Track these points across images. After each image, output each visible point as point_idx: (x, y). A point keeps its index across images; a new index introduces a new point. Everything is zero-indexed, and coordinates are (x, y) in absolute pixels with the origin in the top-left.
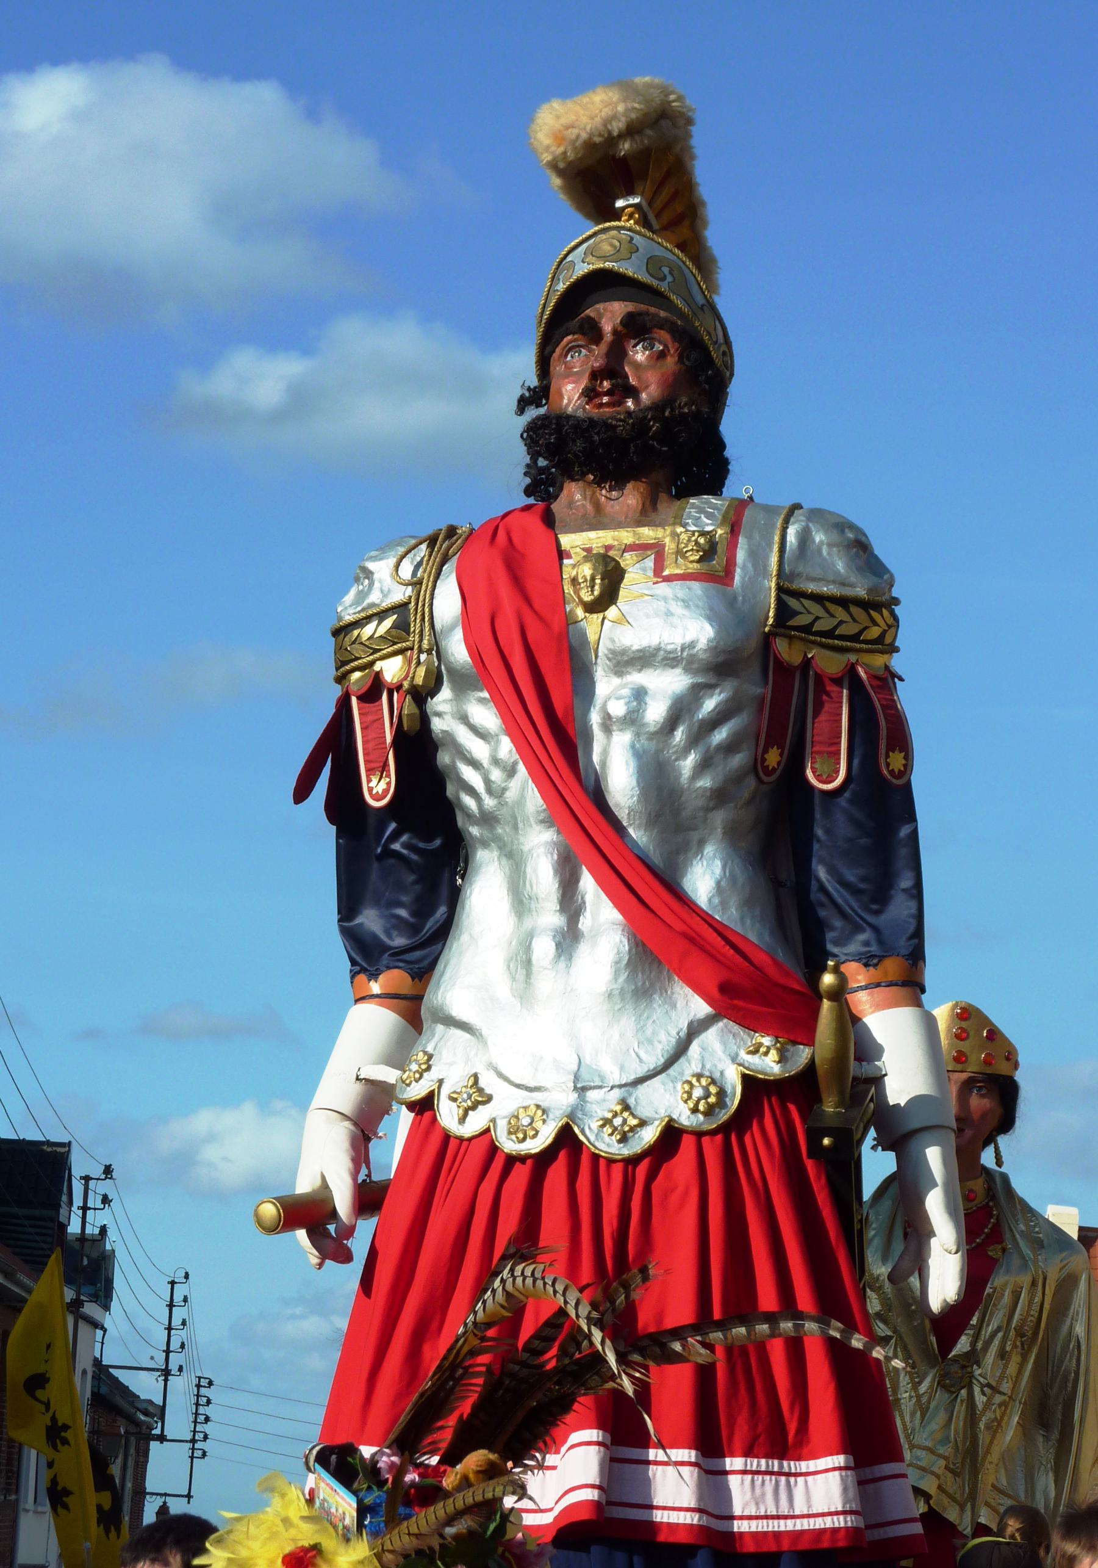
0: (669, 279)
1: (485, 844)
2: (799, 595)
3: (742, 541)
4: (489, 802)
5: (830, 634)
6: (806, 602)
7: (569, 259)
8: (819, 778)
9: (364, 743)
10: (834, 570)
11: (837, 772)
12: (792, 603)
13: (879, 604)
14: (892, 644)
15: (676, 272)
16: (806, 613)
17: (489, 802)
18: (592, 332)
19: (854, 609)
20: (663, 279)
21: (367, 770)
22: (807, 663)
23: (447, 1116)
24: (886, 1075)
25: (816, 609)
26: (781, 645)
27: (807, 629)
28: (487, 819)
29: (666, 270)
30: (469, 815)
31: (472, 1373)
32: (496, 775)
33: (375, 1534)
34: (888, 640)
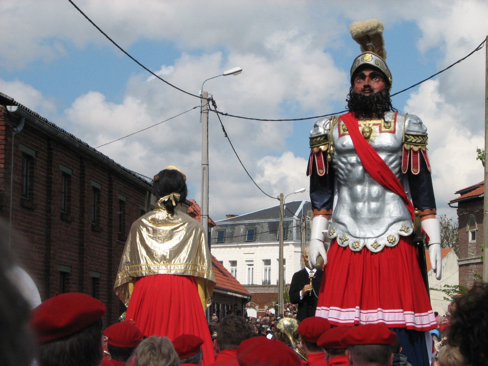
1: (344, 185)
18: (363, 77)
28: (345, 180)
32: (347, 172)
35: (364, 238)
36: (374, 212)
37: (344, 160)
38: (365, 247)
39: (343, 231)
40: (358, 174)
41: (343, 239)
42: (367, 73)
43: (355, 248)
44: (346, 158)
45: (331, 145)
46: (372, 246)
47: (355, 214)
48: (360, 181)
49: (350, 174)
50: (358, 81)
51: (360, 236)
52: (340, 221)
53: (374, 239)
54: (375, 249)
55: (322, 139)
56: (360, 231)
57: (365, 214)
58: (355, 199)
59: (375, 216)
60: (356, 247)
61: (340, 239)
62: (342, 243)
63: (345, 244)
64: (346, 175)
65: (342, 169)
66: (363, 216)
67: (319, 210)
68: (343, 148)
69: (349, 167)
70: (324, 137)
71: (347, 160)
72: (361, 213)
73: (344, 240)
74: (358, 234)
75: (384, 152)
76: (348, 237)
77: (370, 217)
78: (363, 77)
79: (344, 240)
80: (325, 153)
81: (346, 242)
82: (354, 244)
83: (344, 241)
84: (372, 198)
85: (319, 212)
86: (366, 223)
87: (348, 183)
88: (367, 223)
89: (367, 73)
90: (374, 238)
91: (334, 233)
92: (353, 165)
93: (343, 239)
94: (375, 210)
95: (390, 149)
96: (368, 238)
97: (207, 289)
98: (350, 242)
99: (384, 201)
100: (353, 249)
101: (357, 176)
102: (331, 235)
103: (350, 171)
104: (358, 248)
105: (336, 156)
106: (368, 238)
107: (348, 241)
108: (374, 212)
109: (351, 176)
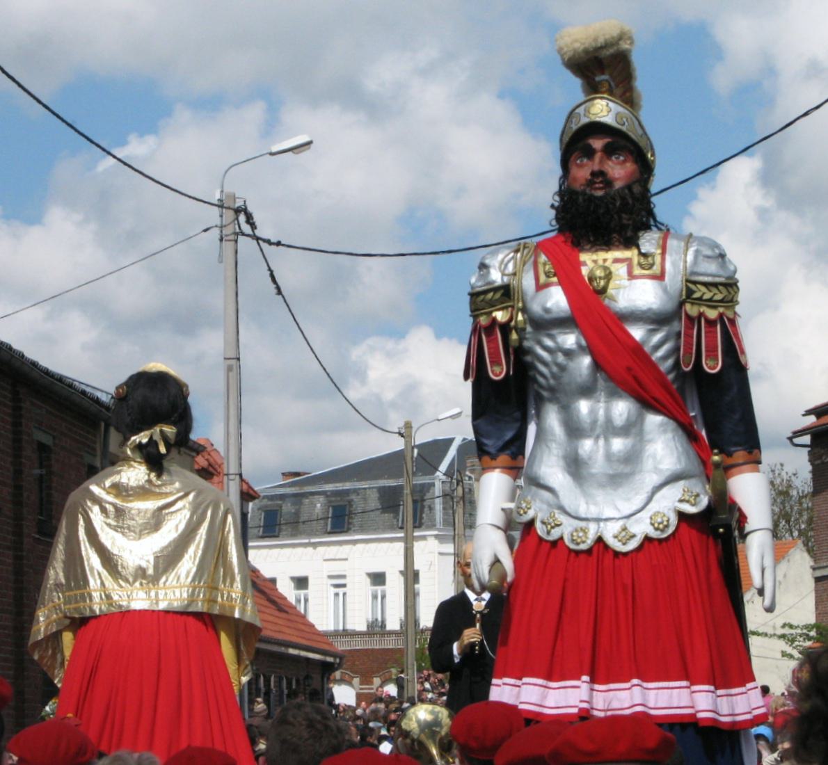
0: (626, 124)
1: (550, 400)
2: (695, 283)
3: (668, 257)
4: (552, 382)
5: (710, 300)
6: (699, 286)
7: (577, 111)
8: (710, 368)
9: (489, 349)
10: (710, 269)
11: (717, 364)
12: (691, 286)
13: (731, 285)
14: (737, 301)
15: (629, 120)
16: (700, 291)
17: (552, 382)
18: (590, 153)
19: (721, 288)
20: (624, 124)
21: (491, 362)
22: (701, 315)
23: (540, 529)
24: (735, 272)
25: (703, 289)
26: (688, 307)
27: (700, 299)
28: (552, 390)
29: (625, 120)
30: (541, 386)
31: (119, 582)
32: (555, 369)
33: (413, 740)
34: (735, 299)
37: (549, 342)
38: (600, 540)
40: (580, 375)
42: (598, 144)
43: (578, 544)
44: (552, 337)
45: (519, 310)
47: (575, 466)
48: (587, 391)
49: (564, 374)
50: (578, 162)
51: (589, 516)
52: (542, 482)
53: (621, 523)
54: (624, 544)
55: (498, 295)
56: (587, 503)
57: (599, 465)
58: (574, 430)
60: (579, 540)
61: (543, 523)
62: (548, 533)
63: (555, 534)
64: (554, 376)
65: (545, 364)
66: (594, 471)
67: (493, 457)
68: (547, 316)
69: (561, 358)
73: (553, 524)
75: (641, 323)
76: (561, 518)
77: (611, 472)
78: (590, 153)
79: (553, 524)
80: (506, 328)
81: (557, 529)
82: (575, 534)
83: (553, 528)
84: (614, 428)
85: (494, 463)
86: (602, 486)
87: (558, 395)
90: (620, 520)
92: (568, 353)
93: (549, 524)
95: (653, 317)
96: (607, 520)
98: (566, 530)
100: (572, 546)
101: (579, 380)
103: (562, 368)
104: (584, 542)
105: (529, 333)
107: (561, 527)
109: (566, 378)
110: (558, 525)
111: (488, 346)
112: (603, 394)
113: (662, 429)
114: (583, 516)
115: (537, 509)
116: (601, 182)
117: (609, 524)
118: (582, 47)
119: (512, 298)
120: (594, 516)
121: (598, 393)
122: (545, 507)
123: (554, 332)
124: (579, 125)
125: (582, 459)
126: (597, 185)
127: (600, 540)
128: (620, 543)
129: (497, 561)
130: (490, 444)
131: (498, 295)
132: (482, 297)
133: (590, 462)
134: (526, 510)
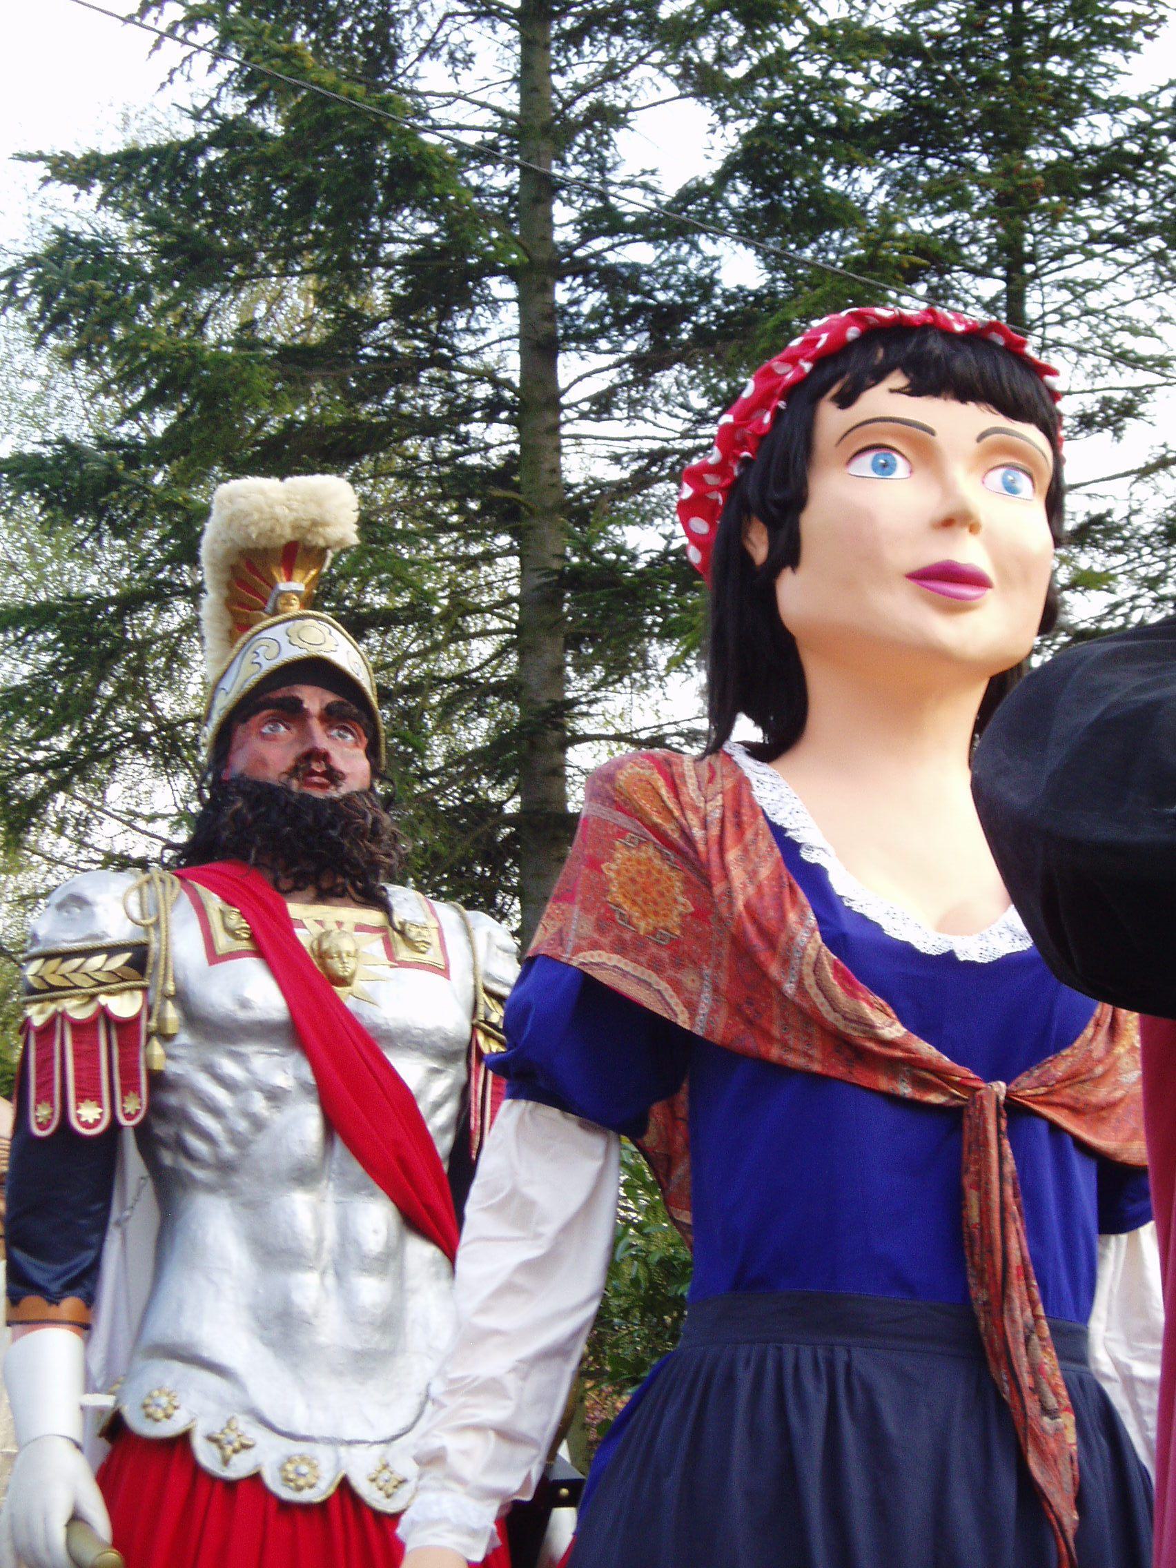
1: (211, 1189)
4: (228, 1150)
18: (293, 712)
28: (225, 1168)
32: (242, 1125)
35: (333, 1442)
36: (371, 1324)
37: (229, 1067)
38: (345, 1486)
39: (222, 1402)
40: (302, 1142)
41: (230, 1443)
42: (314, 700)
43: (299, 1489)
44: (238, 1057)
45: (166, 997)
46: (373, 1480)
47: (282, 1327)
48: (304, 1176)
49: (260, 1137)
50: (266, 730)
51: (315, 1433)
52: (206, 1354)
53: (377, 1449)
54: (388, 1496)
55: (119, 960)
56: (308, 1406)
57: (331, 1329)
58: (274, 1253)
59: (376, 1341)
60: (301, 1482)
61: (211, 1439)
62: (226, 1462)
63: (239, 1468)
64: (236, 1139)
65: (216, 1111)
66: (322, 1339)
67: (54, 1300)
68: (242, 1015)
69: (259, 1104)
70: (128, 955)
71: (248, 1070)
72: (313, 1321)
73: (237, 1445)
74: (300, 1419)
75: (417, 1054)
76: (255, 1433)
77: (357, 1346)
78: (293, 712)
79: (237, 1445)
80: (127, 1029)
81: (244, 1454)
82: (290, 1467)
83: (235, 1451)
84: (363, 1257)
85: (52, 1312)
86: (337, 1373)
87: (236, 1179)
88: (341, 1374)
89: (314, 700)
90: (376, 1447)
91: (176, 1408)
92: (275, 1096)
93: (230, 1443)
94: (379, 1312)
95: (443, 1044)
96: (350, 1443)
97: (1108, 1532)
98: (264, 1458)
99: (400, 1276)
100: (286, 1494)
101: (299, 1151)
102: (157, 1420)
103: (258, 1124)
104: (311, 1486)
105: (184, 1046)
106: (350, 1443)
107: (252, 1452)
108: (371, 1324)
109: (261, 1145)
110: (245, 1447)
111: (76, 1064)
112: (331, 1185)
113: (433, 1270)
114: (303, 1431)
115: (182, 1406)
116: (323, 774)
117: (357, 1451)
118: (291, 517)
119: (149, 971)
120: (327, 1433)
121: (324, 1182)
122: (211, 1407)
123: (248, 1049)
124: (278, 662)
125: (302, 1313)
126: (316, 779)
127: (345, 1486)
128: (382, 1494)
129: (76, 1519)
130: (38, 1271)
131: (119, 960)
132: (77, 962)
133: (315, 1322)
134: (170, 1411)
